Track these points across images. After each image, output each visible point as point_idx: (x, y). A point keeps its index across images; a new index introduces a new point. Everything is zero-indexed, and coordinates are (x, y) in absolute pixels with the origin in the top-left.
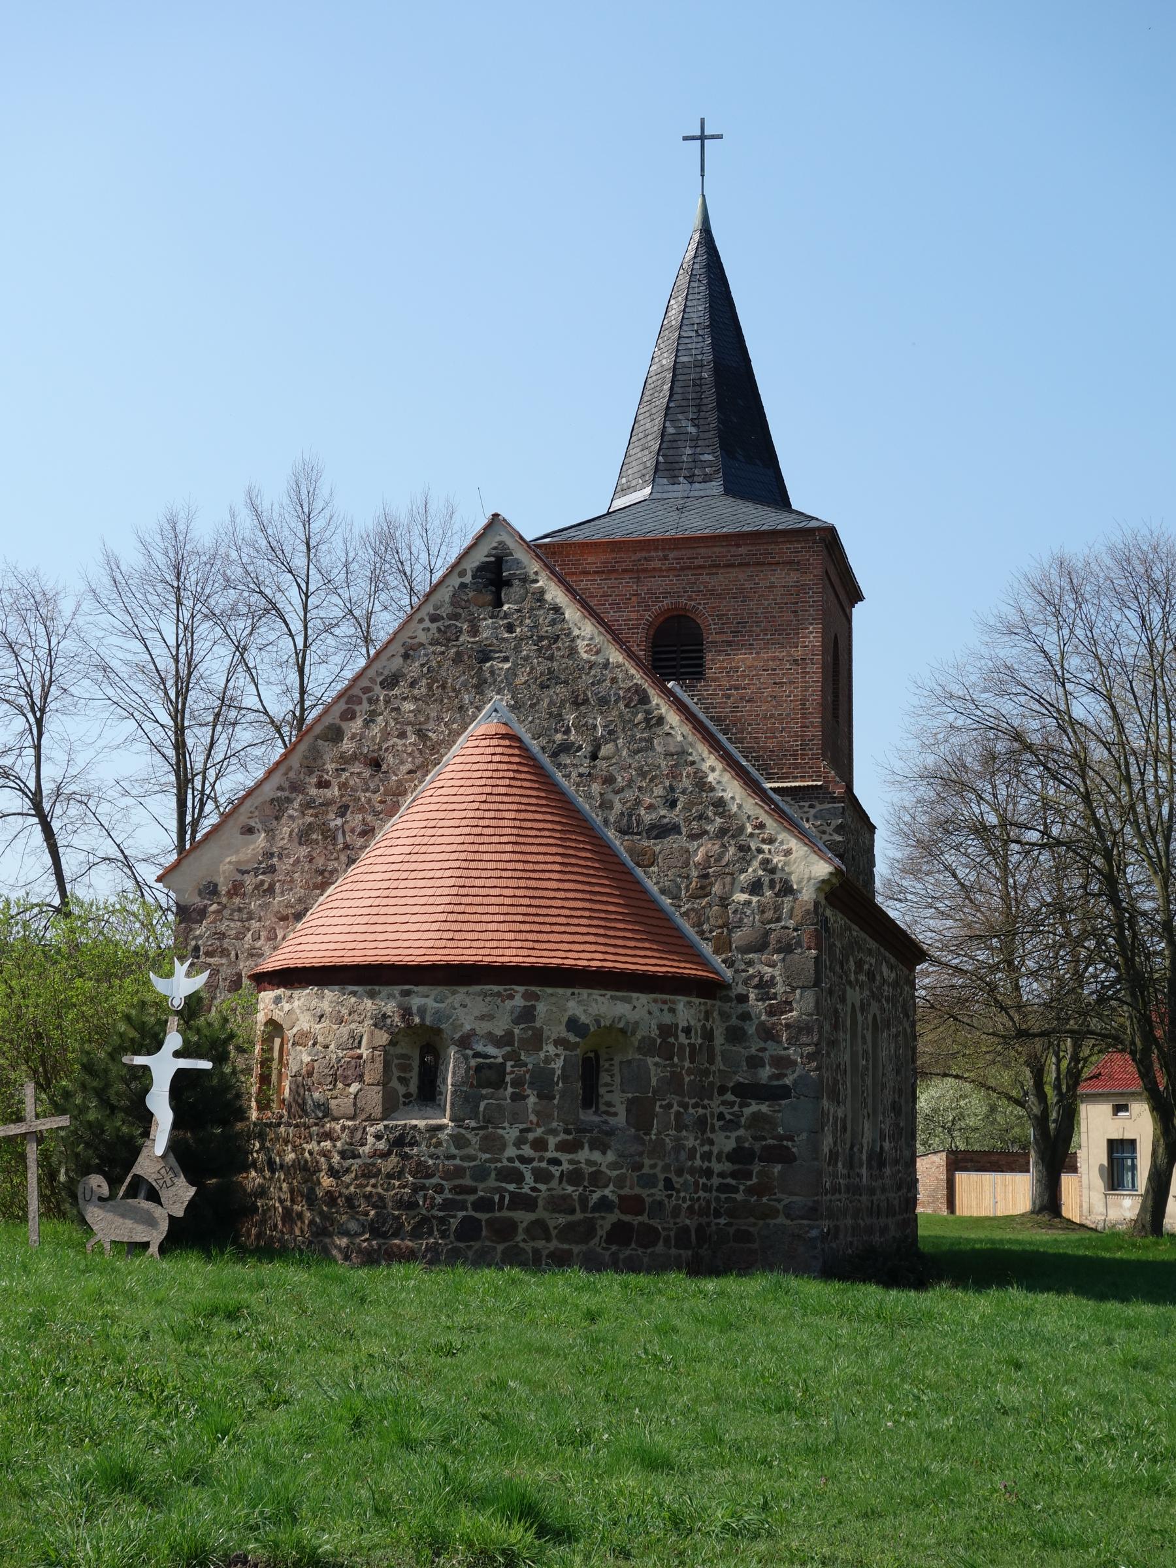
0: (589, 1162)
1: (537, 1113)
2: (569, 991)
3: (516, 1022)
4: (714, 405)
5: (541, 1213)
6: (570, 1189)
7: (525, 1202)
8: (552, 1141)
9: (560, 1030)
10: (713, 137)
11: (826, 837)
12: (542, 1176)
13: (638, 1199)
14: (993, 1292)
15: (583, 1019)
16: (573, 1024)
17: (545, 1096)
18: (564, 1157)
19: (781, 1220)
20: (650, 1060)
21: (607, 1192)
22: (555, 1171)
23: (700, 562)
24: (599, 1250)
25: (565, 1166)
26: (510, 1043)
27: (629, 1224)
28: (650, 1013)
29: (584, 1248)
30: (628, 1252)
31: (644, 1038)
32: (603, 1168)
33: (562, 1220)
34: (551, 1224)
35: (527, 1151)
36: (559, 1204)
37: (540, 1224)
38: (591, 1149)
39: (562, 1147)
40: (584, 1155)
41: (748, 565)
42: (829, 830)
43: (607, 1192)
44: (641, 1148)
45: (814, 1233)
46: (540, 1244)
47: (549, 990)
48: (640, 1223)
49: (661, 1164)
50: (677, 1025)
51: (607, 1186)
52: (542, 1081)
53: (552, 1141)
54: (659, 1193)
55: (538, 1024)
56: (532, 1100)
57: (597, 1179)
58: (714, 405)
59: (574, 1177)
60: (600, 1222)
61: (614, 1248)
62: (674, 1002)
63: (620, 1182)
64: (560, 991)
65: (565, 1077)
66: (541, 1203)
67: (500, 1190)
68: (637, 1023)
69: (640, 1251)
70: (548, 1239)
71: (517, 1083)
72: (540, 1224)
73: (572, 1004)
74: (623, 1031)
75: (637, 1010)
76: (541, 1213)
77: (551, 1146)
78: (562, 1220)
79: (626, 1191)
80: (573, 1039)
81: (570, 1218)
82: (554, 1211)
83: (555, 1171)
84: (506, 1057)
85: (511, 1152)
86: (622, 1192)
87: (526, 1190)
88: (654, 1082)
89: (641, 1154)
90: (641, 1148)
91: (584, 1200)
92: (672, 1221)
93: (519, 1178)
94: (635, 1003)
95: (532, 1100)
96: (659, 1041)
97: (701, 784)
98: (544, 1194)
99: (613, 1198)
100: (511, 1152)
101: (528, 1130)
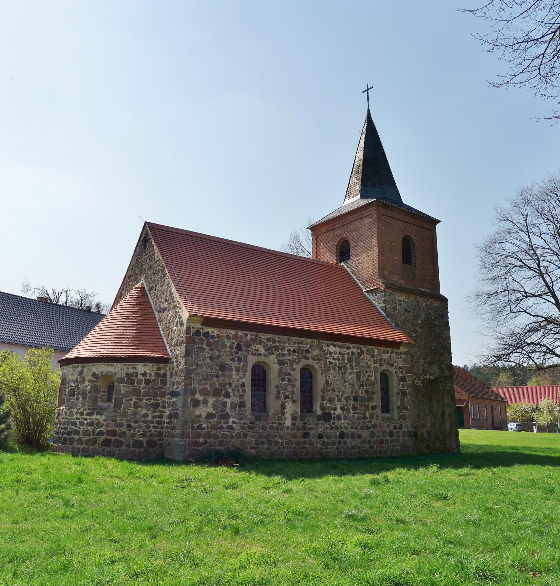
0: (96, 419)
1: (82, 404)
2: (93, 364)
3: (78, 375)
4: (374, 169)
5: (81, 436)
6: (90, 428)
7: (77, 432)
8: (85, 412)
9: (90, 377)
10: (370, 88)
11: (380, 305)
12: (82, 424)
13: (115, 431)
14: (421, 470)
15: (97, 373)
16: (94, 375)
17: (84, 398)
18: (88, 418)
19: (176, 439)
20: (121, 385)
21: (102, 429)
22: (85, 422)
23: (347, 222)
24: (98, 448)
25: (88, 420)
26: (77, 382)
27: (110, 440)
28: (122, 369)
29: (93, 447)
30: (109, 449)
31: (118, 378)
32: (101, 421)
33: (87, 438)
34: (83, 439)
35: (79, 416)
36: (86, 433)
37: (80, 439)
38: (97, 415)
39: (88, 414)
40: (94, 417)
41: (358, 219)
42: (381, 302)
43: (102, 429)
44: (116, 414)
45: (182, 443)
46: (80, 446)
47: (88, 364)
48: (115, 439)
49: (125, 419)
50: (137, 373)
51: (102, 427)
52: (84, 394)
53: (85, 412)
54: (124, 429)
55: (84, 376)
56: (81, 399)
57: (99, 424)
58: (374, 169)
59: (91, 424)
60: (99, 439)
61: (104, 447)
62: (135, 365)
63: (107, 426)
64: (91, 364)
65: (90, 392)
66: (81, 432)
67: (72, 428)
68: (116, 373)
69: (114, 449)
70: (82, 444)
71: (78, 395)
72: (80, 439)
73: (94, 368)
74: (111, 376)
75: (118, 369)
76: (81, 436)
77: (85, 414)
78: (87, 438)
79: (109, 429)
80: (93, 379)
81: (89, 437)
82: (84, 435)
83: (85, 422)
84: (76, 387)
85: (75, 416)
86: (108, 429)
87: (77, 428)
88: (123, 392)
89: (116, 416)
90: (116, 414)
91: (94, 432)
92: (131, 439)
93: (75, 424)
94: (115, 366)
95: (81, 399)
96: (126, 379)
97: (171, 294)
98: (82, 430)
99: (105, 431)
100: (75, 416)
101: (79, 409)
